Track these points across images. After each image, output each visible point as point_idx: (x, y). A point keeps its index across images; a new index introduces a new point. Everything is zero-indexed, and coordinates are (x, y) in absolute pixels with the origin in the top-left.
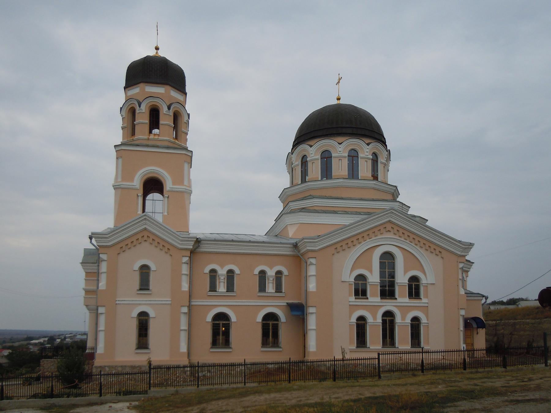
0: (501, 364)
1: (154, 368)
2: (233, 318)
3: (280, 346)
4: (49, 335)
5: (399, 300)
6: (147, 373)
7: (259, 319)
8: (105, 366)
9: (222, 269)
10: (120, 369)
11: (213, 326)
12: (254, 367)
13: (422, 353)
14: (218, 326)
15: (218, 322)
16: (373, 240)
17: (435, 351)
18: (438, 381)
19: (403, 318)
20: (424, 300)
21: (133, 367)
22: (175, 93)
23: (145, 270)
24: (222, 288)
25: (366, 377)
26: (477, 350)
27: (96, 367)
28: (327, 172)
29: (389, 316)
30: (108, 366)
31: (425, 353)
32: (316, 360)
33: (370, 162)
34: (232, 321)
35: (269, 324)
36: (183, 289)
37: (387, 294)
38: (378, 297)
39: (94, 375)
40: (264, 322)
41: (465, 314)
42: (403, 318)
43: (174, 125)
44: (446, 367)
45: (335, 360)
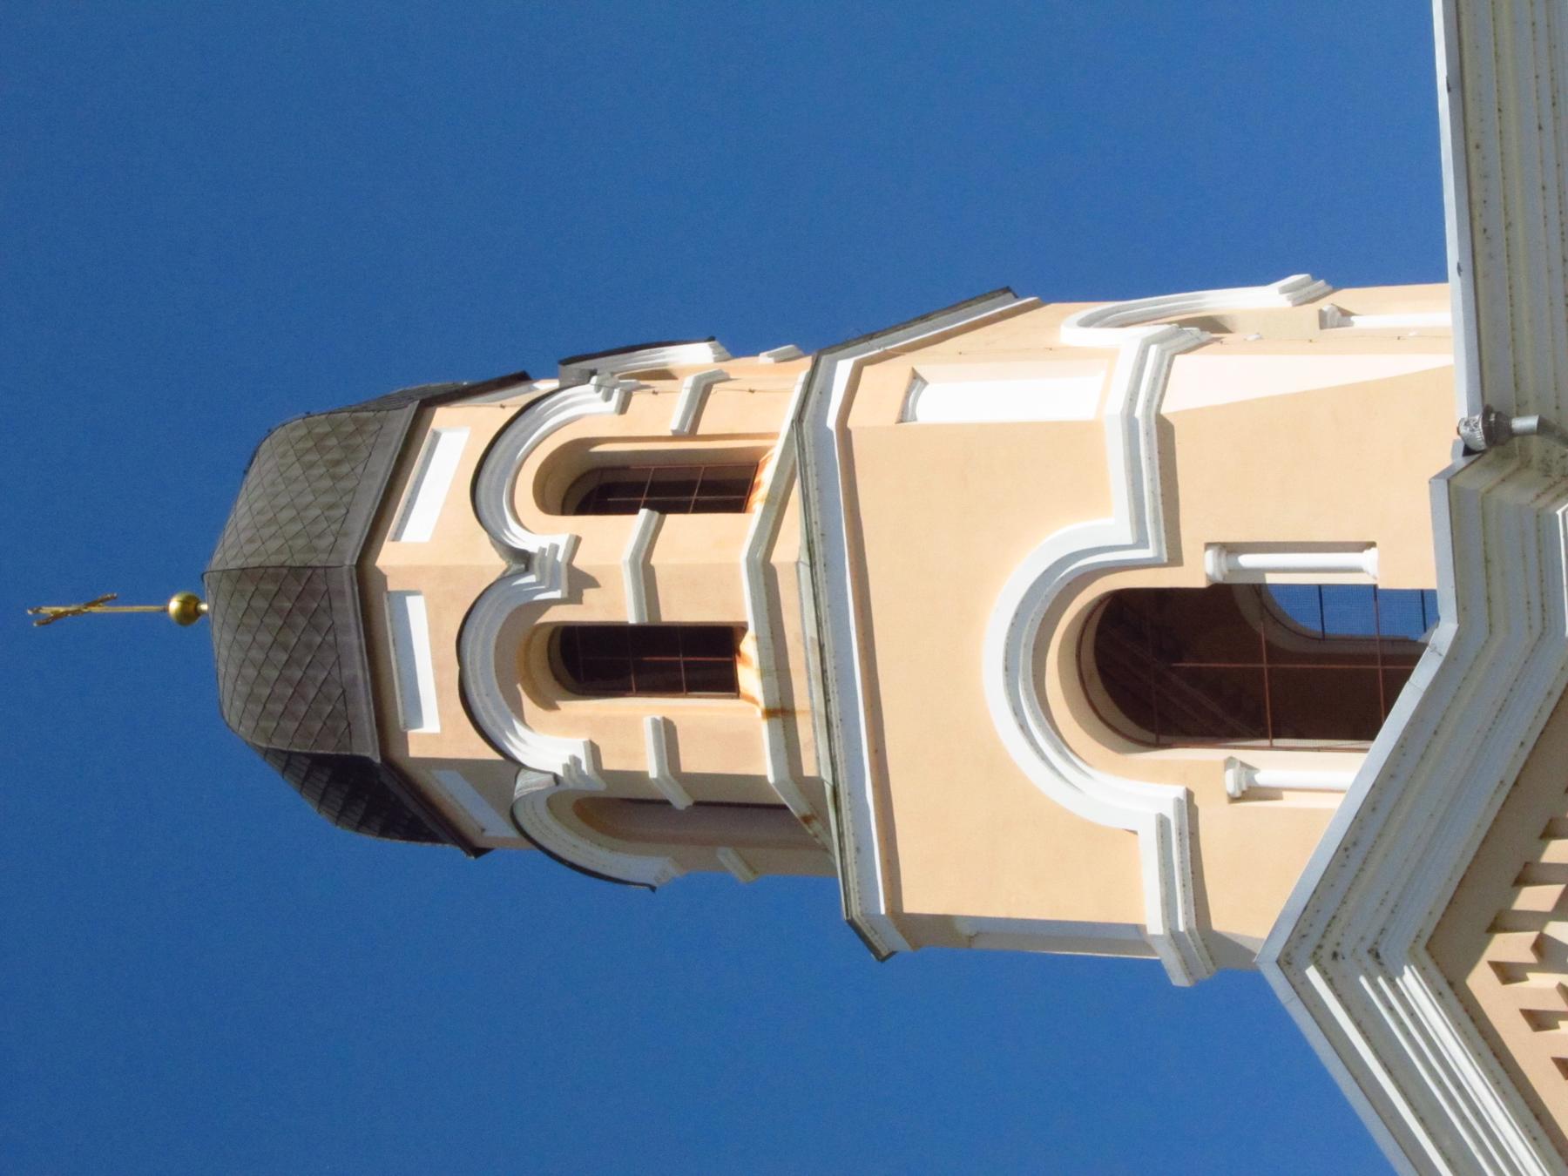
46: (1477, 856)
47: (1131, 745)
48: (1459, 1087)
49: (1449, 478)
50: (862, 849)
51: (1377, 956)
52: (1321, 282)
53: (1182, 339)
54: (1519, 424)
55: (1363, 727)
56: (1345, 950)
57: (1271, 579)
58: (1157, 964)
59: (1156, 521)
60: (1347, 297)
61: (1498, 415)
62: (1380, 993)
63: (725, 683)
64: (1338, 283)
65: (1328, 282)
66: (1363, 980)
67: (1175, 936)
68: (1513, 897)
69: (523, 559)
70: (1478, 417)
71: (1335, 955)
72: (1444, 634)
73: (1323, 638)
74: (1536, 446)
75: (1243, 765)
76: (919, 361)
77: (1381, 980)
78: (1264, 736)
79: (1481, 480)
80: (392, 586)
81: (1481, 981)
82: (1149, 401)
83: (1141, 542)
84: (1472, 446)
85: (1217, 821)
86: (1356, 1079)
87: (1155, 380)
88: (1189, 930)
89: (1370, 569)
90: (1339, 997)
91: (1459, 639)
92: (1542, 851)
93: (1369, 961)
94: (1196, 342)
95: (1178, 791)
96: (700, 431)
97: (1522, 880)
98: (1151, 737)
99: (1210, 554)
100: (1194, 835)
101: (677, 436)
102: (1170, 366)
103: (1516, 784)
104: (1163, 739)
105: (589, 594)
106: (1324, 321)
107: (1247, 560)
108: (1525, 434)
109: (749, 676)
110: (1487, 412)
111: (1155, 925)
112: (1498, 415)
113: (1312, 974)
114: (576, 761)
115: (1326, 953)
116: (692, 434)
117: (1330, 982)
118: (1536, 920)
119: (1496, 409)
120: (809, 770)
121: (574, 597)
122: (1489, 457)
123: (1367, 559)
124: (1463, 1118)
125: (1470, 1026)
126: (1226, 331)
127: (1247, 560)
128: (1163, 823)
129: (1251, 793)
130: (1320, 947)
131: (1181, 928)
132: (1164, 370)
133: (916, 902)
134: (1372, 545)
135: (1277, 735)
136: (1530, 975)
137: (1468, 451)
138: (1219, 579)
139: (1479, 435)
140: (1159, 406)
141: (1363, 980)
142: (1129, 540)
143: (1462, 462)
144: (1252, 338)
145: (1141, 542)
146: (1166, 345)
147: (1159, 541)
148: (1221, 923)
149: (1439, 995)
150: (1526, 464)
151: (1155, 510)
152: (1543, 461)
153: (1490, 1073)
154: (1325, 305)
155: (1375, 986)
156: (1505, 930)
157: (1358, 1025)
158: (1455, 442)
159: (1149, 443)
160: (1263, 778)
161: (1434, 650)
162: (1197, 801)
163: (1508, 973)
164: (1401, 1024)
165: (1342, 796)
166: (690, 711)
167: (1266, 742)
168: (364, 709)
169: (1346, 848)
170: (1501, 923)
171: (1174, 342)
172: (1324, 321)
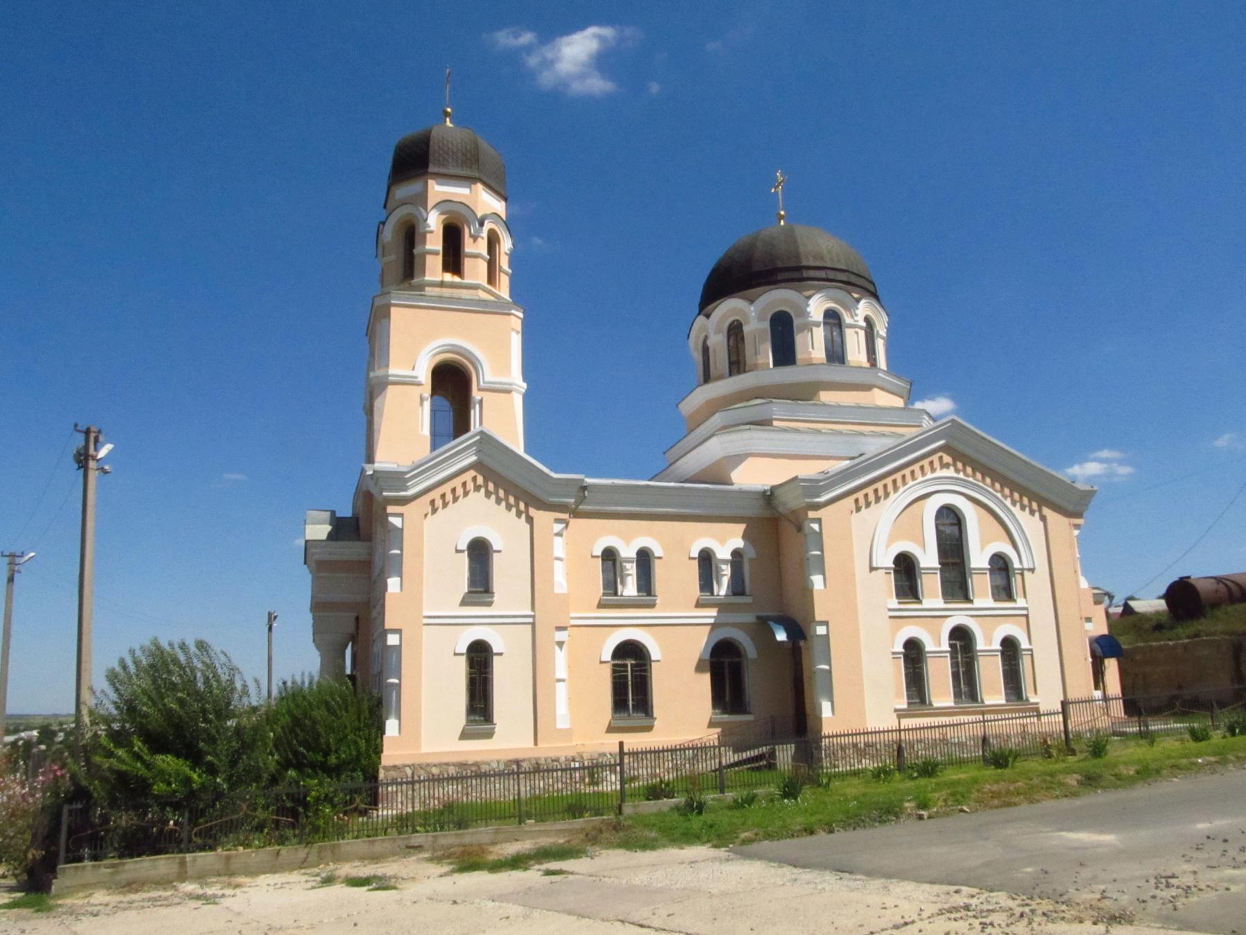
1: (629, 754)
2: (655, 652)
4: (39, 721)
5: (978, 603)
6: (1058, 713)
7: (607, 655)
8: (405, 766)
9: (628, 546)
10: (435, 771)
11: (614, 671)
16: (910, 487)
17: (862, 731)
19: (989, 640)
20: (1021, 602)
21: (462, 765)
22: (489, 196)
23: (480, 552)
24: (630, 588)
25: (545, 814)
26: (1113, 699)
27: (385, 768)
28: (785, 353)
29: (961, 636)
30: (409, 766)
33: (862, 334)
35: (626, 666)
36: (556, 591)
38: (938, 597)
39: (825, 737)
42: (989, 640)
43: (488, 257)
44: (637, 791)
50: (407, 299)
54: (586, 493)
55: (528, 449)
57: (472, 412)
63: (777, 363)
69: (482, 224)
76: (520, 334)
80: (473, 186)
85: (416, 391)
91: (551, 477)
95: (423, 382)
96: (501, 274)
97: (495, 484)
101: (500, 267)
105: (472, 240)
107: (477, 406)
109: (448, 277)
114: (429, 227)
116: (500, 271)
120: (427, 289)
121: (471, 236)
127: (477, 406)
128: (416, 377)
133: (393, 310)
142: (486, 379)
145: (484, 382)
148: (390, 388)
163: (474, 479)
166: (439, 260)
168: (442, 170)
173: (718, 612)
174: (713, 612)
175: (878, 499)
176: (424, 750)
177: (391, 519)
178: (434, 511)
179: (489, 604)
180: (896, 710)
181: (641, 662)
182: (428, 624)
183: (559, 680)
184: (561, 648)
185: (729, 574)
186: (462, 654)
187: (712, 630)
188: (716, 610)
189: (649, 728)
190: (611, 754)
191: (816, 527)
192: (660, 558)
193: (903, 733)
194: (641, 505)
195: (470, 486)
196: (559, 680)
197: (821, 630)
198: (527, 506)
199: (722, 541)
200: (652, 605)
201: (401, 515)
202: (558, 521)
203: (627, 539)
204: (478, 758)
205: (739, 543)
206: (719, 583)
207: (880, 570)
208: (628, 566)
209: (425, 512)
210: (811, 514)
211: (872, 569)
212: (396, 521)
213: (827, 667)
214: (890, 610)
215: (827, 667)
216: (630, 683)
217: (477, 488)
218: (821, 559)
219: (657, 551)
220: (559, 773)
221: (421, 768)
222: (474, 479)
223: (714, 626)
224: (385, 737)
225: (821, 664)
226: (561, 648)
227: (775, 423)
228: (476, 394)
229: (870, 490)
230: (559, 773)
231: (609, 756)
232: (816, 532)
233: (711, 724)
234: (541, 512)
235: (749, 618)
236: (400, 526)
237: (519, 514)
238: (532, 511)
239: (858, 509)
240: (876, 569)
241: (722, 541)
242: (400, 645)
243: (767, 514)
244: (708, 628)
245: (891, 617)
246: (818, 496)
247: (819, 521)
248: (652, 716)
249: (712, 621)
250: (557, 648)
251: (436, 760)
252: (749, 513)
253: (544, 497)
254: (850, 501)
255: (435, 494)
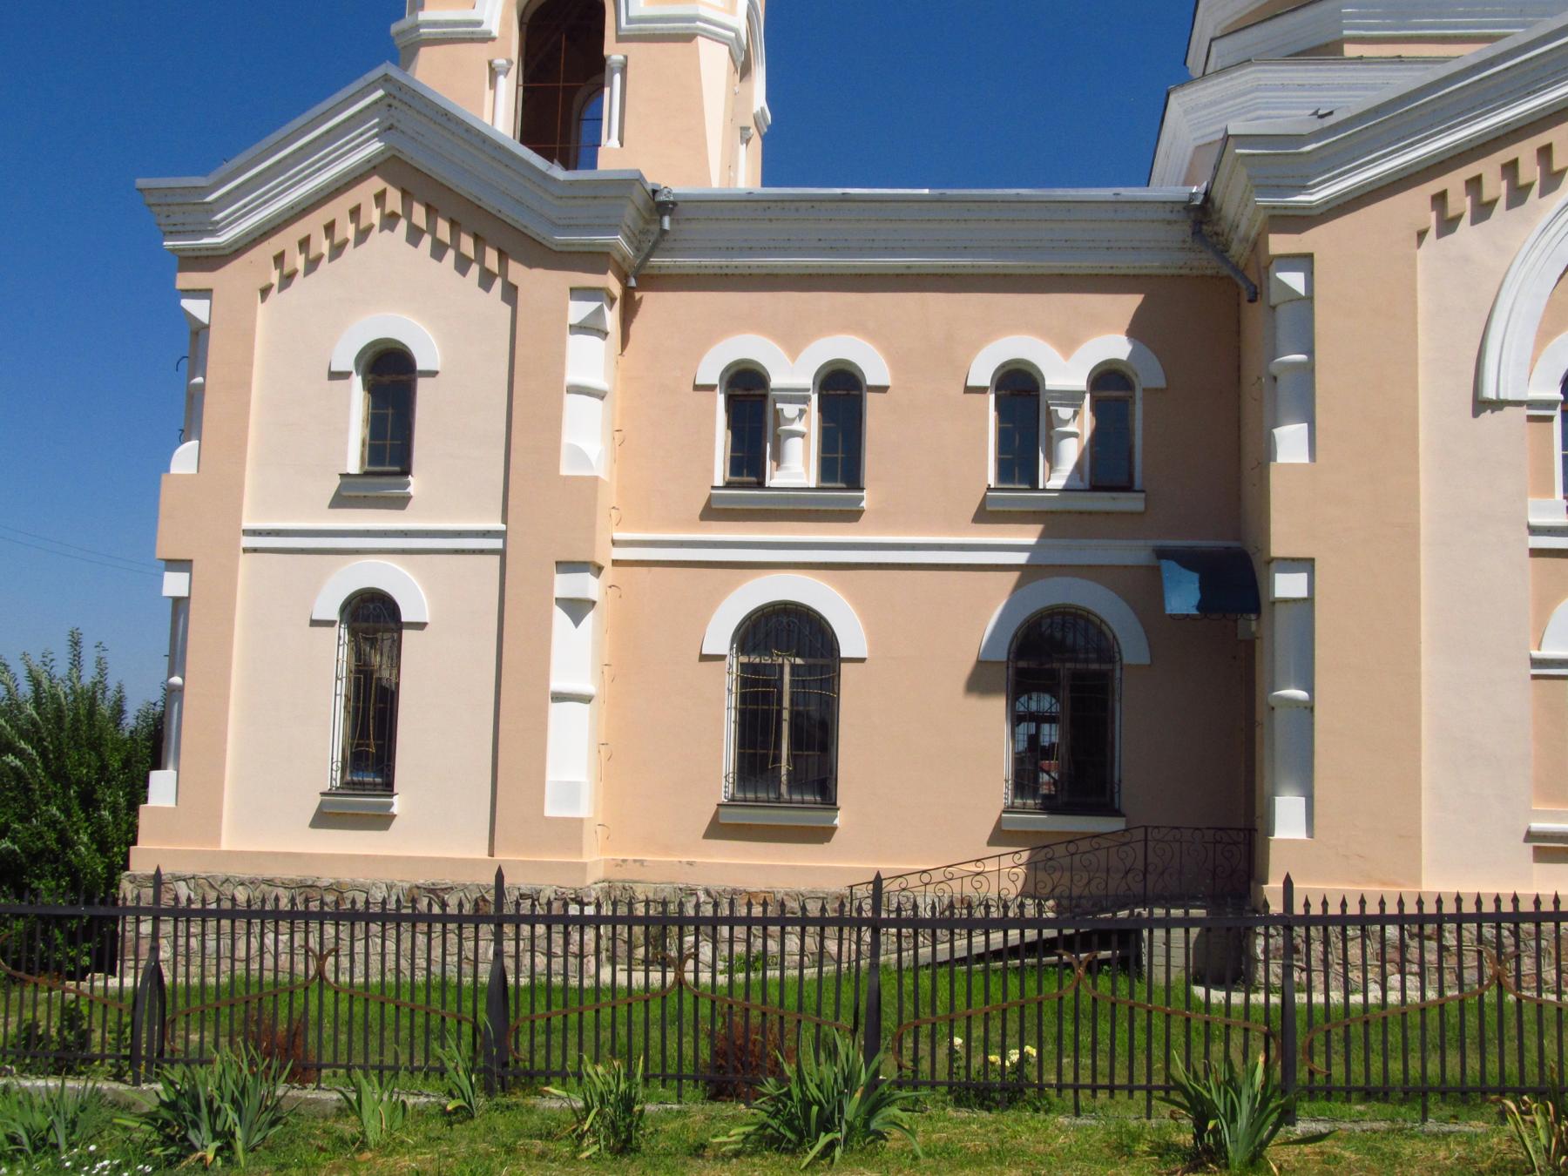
0: (1112, 1075)
2: (851, 638)
3: (1117, 806)
7: (719, 636)
11: (744, 683)
12: (195, 969)
13: (876, 926)
14: (767, 683)
15: (767, 660)
18: (1257, 1142)
21: (306, 888)
31: (899, 923)
32: (1344, 904)
34: (1125, 661)
37: (381, 442)
40: (1022, 664)
41: (162, 577)
45: (1299, 910)
46: (442, 184)
47: (523, 5)
48: (319, 169)
49: (639, 180)
51: (390, 129)
52: (766, 130)
53: (738, 51)
56: (393, 111)
57: (607, 90)
58: (402, 16)
59: (640, 29)
60: (756, 143)
61: (672, 209)
62: (370, 129)
64: (765, 139)
65: (766, 134)
66: (376, 120)
67: (418, 26)
68: (420, 202)
70: (672, 198)
71: (390, 106)
72: (558, 172)
73: (580, 120)
74: (655, 228)
75: (509, 69)
77: (376, 130)
78: (525, 81)
79: (638, 197)
81: (376, 184)
82: (705, 30)
83: (629, 21)
84: (658, 194)
85: (480, 53)
86: (323, 113)
87: (716, 34)
88: (420, 35)
89: (609, 143)
90: (367, 107)
91: (555, 180)
92: (492, 247)
93: (387, 124)
94: (736, 58)
95: (495, 33)
98: (526, 20)
99: (622, 58)
100: (472, 40)
102: (723, 43)
103: (479, 207)
104: (525, 27)
106: (744, 129)
107: (617, 78)
108: (661, 222)
110: (674, 203)
111: (423, 16)
112: (672, 209)
113: (380, 93)
115: (391, 101)
117: (375, 102)
118: (408, 214)
119: (676, 208)
122: (651, 203)
123: (614, 142)
124: (302, 170)
125: (353, 176)
126: (741, 80)
127: (617, 78)
128: (479, 23)
129: (494, 73)
130: (394, 98)
131: (421, 31)
132: (709, 35)
134: (622, 145)
135: (525, 90)
136: (379, 210)
137: (655, 192)
138: (608, 62)
139: (662, 198)
140: (703, 36)
141: (376, 120)
143: (649, 188)
144: (736, 89)
145: (629, 21)
146: (735, 42)
147: (630, 30)
148: (425, 53)
149: (369, 161)
150: (647, 222)
151: (645, 30)
152: (648, 231)
153: (328, 186)
154: (753, 130)
155: (373, 127)
156: (403, 197)
157: (352, 117)
158: (659, 185)
159: (682, 28)
160: (501, 80)
161: (550, 167)
162: (490, 43)
163: (380, 198)
164: (353, 140)
165: (490, 123)
167: (521, 82)
169: (460, 123)
170: (407, 196)
171: (735, 45)
172: (744, 129)
173: (1043, 536)
174: (1028, 535)
175: (1518, 194)
176: (229, 841)
177: (187, 304)
178: (287, 279)
179: (401, 502)
180: (1530, 836)
181: (821, 661)
182: (255, 550)
183: (559, 697)
184: (577, 621)
185: (1087, 434)
186: (330, 623)
187: (1019, 585)
188: (1039, 528)
189: (823, 834)
190: (708, 893)
191: (1295, 280)
192: (883, 389)
193: (889, 936)
194: (833, 250)
195: (374, 216)
196: (559, 697)
197: (1288, 585)
198: (503, 256)
199: (1067, 344)
200: (852, 515)
201: (205, 293)
202: (579, 293)
203: (793, 345)
204: (345, 875)
205: (1116, 346)
206: (1052, 460)
207: (1508, 410)
208: (790, 410)
209: (263, 284)
210: (1279, 244)
211: (1481, 405)
212: (197, 308)
213: (1301, 694)
214: (1534, 531)
215: (1301, 694)
216: (786, 715)
217: (390, 221)
218: (1307, 372)
219: (875, 370)
220: (541, 929)
221: (212, 886)
222: (380, 198)
223: (1028, 573)
224: (143, 809)
225: (1288, 687)
226: (577, 621)
227: (1350, 50)
228: (613, 51)
229: (1489, 168)
230: (541, 929)
231: (703, 897)
232: (1299, 298)
233: (1000, 836)
234: (538, 273)
235: (1131, 552)
236: (204, 318)
237: (486, 280)
238: (517, 272)
239: (1447, 225)
240: (1498, 405)
241: (1067, 344)
242: (188, 598)
243: (1204, 262)
244: (1015, 575)
245: (1536, 553)
246: (1303, 188)
247: (1304, 262)
248: (835, 804)
249: (1021, 558)
250: (560, 617)
251: (246, 872)
252: (1151, 263)
253: (536, 229)
254: (1414, 204)
255: (286, 240)
